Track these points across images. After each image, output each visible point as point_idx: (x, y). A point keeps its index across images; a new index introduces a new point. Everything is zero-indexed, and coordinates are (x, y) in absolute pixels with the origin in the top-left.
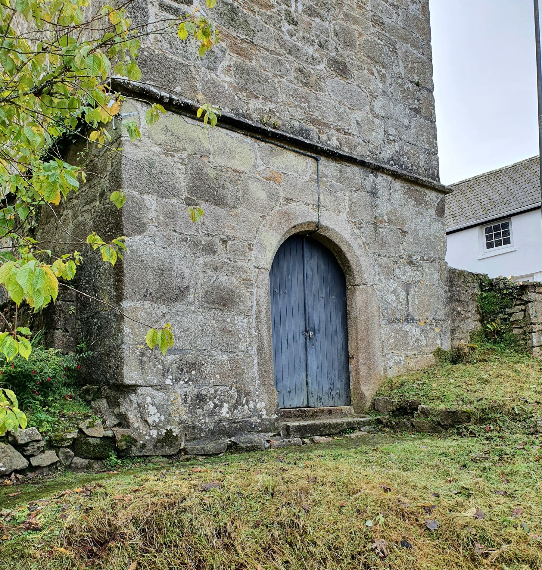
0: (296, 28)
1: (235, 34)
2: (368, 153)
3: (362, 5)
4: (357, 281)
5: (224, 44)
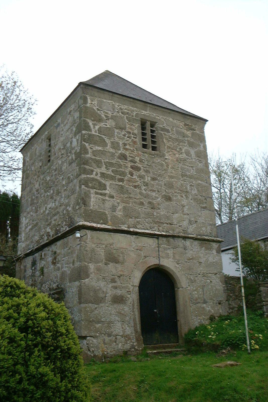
0: (148, 187)
1: (122, 196)
2: (181, 231)
3: (176, 170)
4: (179, 286)
5: (118, 201)
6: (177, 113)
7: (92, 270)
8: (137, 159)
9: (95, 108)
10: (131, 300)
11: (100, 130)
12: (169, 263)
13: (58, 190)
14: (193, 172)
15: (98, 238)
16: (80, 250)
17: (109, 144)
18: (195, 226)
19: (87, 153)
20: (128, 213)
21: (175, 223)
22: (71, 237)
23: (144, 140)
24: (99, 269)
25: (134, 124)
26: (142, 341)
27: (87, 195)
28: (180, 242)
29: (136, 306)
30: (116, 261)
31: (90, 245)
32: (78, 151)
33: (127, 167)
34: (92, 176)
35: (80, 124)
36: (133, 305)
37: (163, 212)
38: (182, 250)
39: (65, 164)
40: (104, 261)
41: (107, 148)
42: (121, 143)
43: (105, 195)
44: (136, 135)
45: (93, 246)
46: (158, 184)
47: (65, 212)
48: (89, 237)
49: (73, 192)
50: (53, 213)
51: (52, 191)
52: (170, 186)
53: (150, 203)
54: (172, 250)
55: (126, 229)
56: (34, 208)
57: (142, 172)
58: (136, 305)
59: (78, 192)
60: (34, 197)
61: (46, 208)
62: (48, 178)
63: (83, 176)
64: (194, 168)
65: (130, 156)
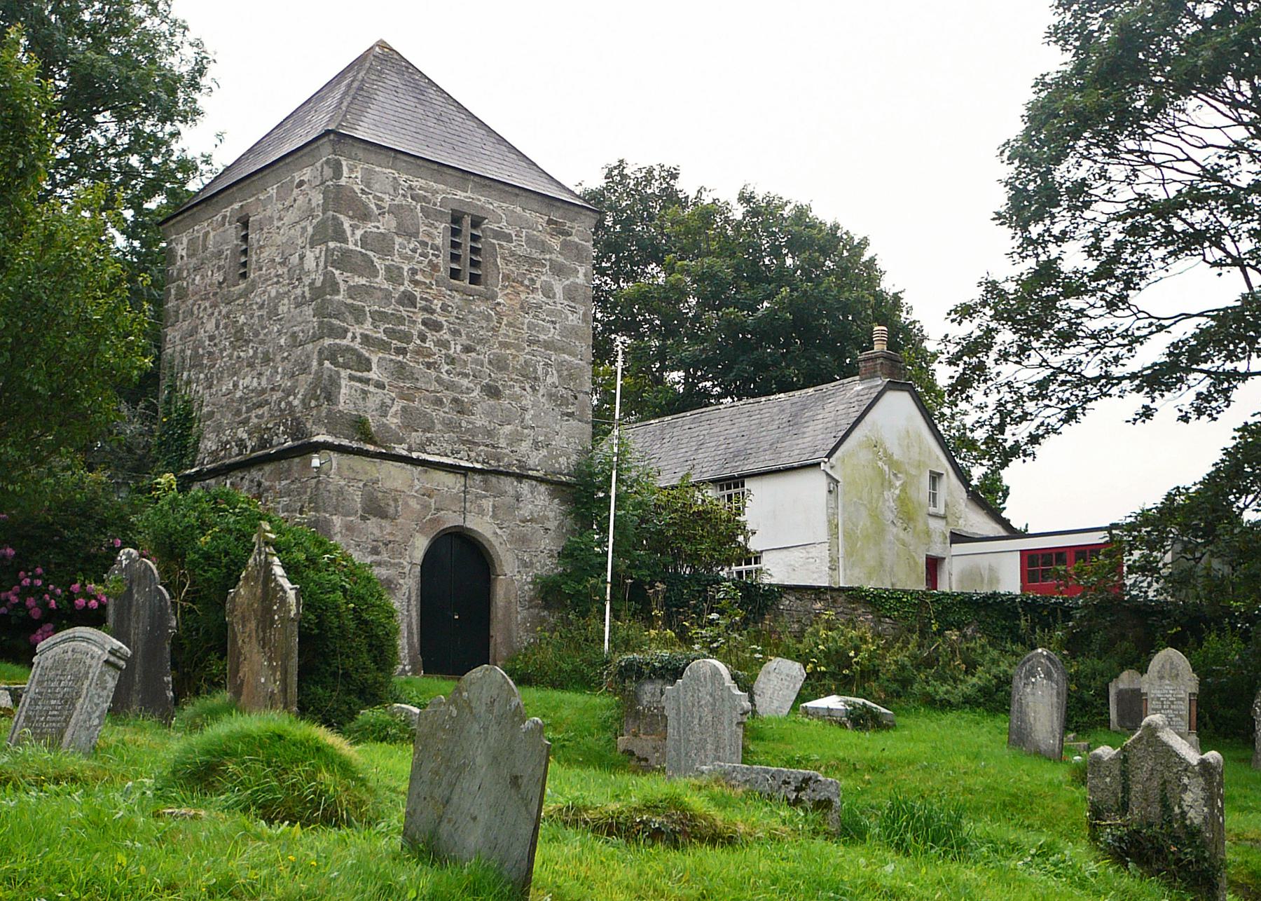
6: (533, 196)
7: (337, 529)
8: (437, 305)
9: (356, 188)
10: (405, 589)
11: (364, 241)
12: (482, 525)
13: (266, 354)
14: (553, 334)
15: (350, 468)
16: (317, 487)
17: (382, 272)
18: (544, 452)
19: (338, 292)
20: (411, 419)
21: (504, 445)
22: (297, 460)
23: (455, 258)
24: (349, 528)
25: (437, 224)
26: (419, 665)
27: (334, 382)
28: (508, 485)
29: (413, 602)
30: (384, 515)
31: (336, 481)
32: (318, 284)
33: (414, 322)
34: (344, 342)
35: (323, 223)
36: (409, 599)
37: (480, 421)
38: (513, 501)
39: (286, 301)
40: (360, 512)
41: (378, 280)
42: (406, 269)
43: (367, 381)
44: (438, 249)
45: (342, 483)
46: (476, 362)
47: (283, 405)
48: (334, 465)
49: (305, 369)
50: (255, 400)
51: (251, 352)
52: (500, 364)
53: (455, 400)
54: (491, 499)
55: (405, 453)
56: (202, 376)
57: (445, 335)
58: (413, 599)
59: (316, 373)
60: (201, 351)
61: (235, 385)
62: (242, 319)
63: (327, 342)
64: (557, 326)
65: (422, 299)
